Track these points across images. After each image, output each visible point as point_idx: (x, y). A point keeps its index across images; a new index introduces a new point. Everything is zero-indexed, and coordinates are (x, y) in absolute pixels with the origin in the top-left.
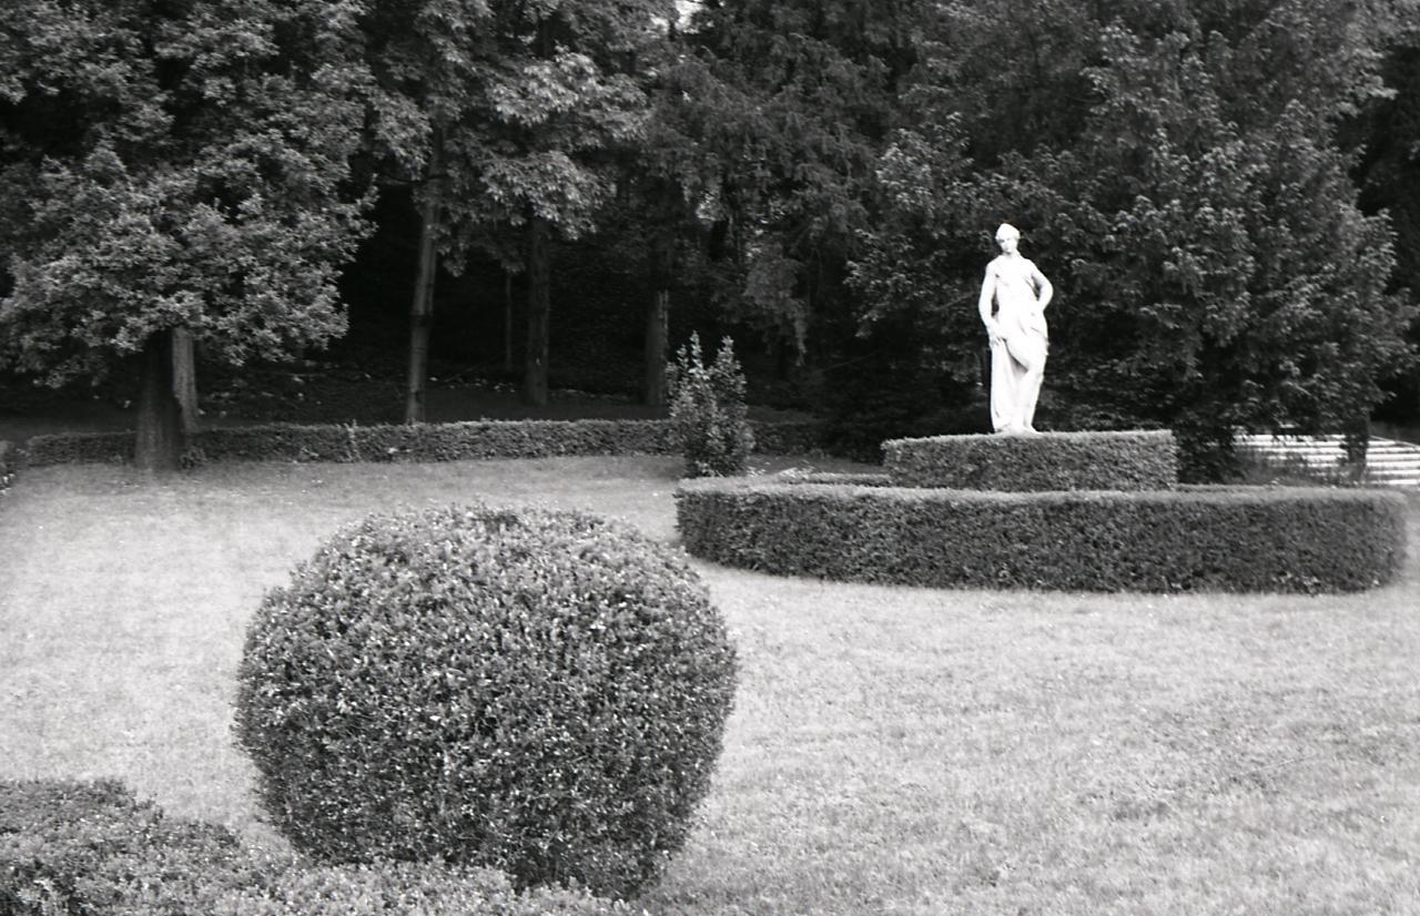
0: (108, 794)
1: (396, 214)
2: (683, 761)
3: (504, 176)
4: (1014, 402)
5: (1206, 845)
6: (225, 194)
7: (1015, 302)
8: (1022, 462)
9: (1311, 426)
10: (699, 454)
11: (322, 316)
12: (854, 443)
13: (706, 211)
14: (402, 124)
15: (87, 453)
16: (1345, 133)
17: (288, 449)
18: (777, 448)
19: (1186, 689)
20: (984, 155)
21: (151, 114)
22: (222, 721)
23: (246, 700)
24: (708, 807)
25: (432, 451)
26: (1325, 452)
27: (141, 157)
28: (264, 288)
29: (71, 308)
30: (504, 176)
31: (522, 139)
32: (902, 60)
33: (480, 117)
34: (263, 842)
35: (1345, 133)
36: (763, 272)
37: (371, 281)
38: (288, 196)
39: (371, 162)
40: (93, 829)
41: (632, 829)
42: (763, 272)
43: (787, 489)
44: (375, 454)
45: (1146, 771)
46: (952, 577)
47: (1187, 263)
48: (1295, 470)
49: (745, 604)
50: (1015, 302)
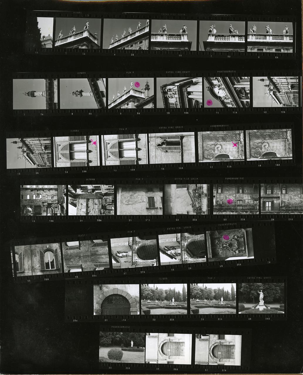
0: (103, 357)
1: (113, 340)
2: (122, 357)
3: (276, 297)
4: (132, 346)
5: (138, 360)
6: (107, 339)
7: (132, 343)
8: (132, 348)
9: (141, 347)
10: (122, 347)
11: (110, 343)
12: (127, 347)
13: (122, 340)
14: (113, 337)
15: (103, 347)
16: (142, 338)
17: (109, 347)
18: (125, 347)
19: (137, 355)
20: (131, 338)
21: (105, 336)
22: (107, 355)
23: (108, 354)
24: (122, 358)
25: (114, 347)
26: (142, 348)
27: (105, 338)
28: (109, 342)
29: (102, 342)
30: (276, 297)
31: (117, 337)
32: (129, 335)
33: (115, 337)
34: (108, 359)
35: (142, 338)
36: (124, 342)
37: (112, 341)
38: (109, 339)
39: (112, 338)
40: (103, 358)
41: (120, 359)
42: (124, 342)
43: (227, 49)
44: (112, 347)
45: (136, 357)
46: (130, 351)
47: (137, 342)
48: (141, 348)
49: (123, 352)
50: (132, 343)
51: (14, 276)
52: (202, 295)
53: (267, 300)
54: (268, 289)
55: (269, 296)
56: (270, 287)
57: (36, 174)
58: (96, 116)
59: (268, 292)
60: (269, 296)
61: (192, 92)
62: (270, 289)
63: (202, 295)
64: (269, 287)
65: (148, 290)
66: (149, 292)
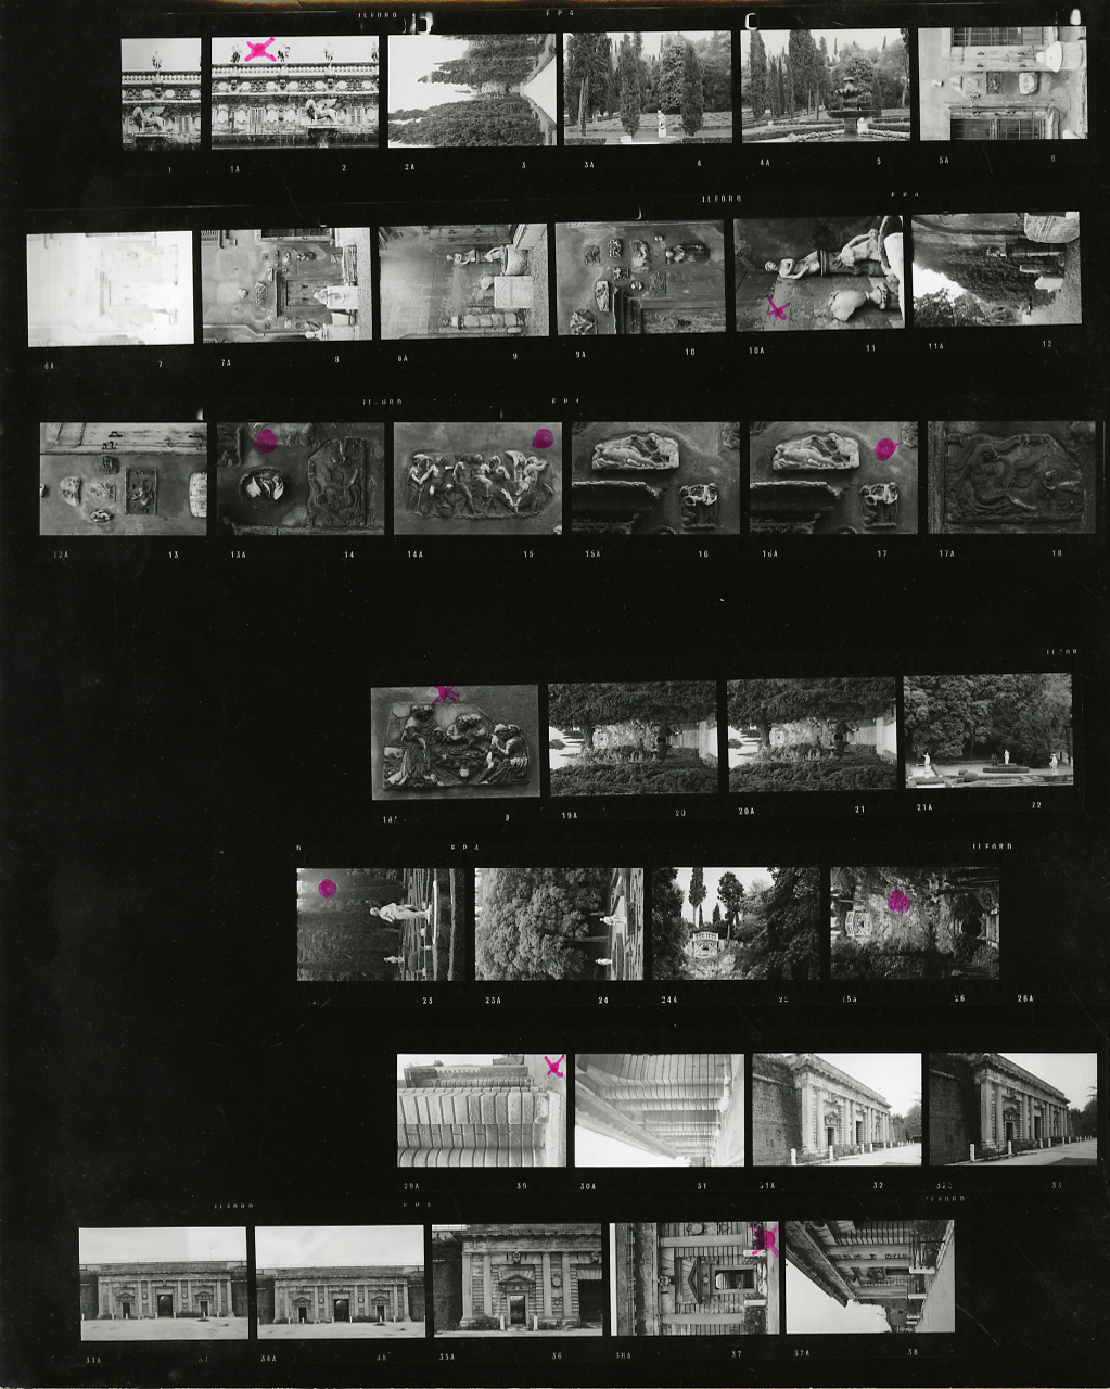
4: (1007, 762)
11: (961, 754)
27: (947, 742)
38: (958, 745)
51: (251, 1205)
52: (566, 885)
53: (941, 751)
54: (945, 714)
55: (950, 736)
56: (951, 709)
57: (519, 1188)
58: (559, 13)
59: (945, 727)
60: (950, 736)
61: (437, 77)
62: (954, 716)
63: (566, 885)
64: (947, 706)
65: (506, 931)
66: (521, 921)
